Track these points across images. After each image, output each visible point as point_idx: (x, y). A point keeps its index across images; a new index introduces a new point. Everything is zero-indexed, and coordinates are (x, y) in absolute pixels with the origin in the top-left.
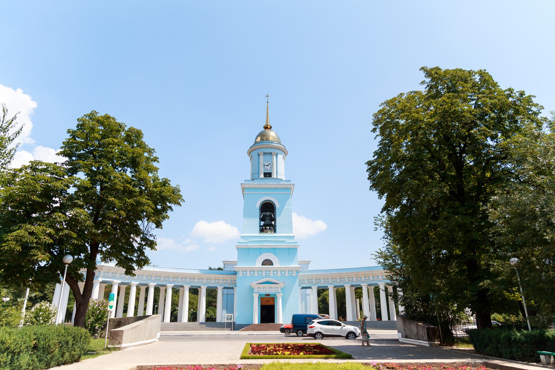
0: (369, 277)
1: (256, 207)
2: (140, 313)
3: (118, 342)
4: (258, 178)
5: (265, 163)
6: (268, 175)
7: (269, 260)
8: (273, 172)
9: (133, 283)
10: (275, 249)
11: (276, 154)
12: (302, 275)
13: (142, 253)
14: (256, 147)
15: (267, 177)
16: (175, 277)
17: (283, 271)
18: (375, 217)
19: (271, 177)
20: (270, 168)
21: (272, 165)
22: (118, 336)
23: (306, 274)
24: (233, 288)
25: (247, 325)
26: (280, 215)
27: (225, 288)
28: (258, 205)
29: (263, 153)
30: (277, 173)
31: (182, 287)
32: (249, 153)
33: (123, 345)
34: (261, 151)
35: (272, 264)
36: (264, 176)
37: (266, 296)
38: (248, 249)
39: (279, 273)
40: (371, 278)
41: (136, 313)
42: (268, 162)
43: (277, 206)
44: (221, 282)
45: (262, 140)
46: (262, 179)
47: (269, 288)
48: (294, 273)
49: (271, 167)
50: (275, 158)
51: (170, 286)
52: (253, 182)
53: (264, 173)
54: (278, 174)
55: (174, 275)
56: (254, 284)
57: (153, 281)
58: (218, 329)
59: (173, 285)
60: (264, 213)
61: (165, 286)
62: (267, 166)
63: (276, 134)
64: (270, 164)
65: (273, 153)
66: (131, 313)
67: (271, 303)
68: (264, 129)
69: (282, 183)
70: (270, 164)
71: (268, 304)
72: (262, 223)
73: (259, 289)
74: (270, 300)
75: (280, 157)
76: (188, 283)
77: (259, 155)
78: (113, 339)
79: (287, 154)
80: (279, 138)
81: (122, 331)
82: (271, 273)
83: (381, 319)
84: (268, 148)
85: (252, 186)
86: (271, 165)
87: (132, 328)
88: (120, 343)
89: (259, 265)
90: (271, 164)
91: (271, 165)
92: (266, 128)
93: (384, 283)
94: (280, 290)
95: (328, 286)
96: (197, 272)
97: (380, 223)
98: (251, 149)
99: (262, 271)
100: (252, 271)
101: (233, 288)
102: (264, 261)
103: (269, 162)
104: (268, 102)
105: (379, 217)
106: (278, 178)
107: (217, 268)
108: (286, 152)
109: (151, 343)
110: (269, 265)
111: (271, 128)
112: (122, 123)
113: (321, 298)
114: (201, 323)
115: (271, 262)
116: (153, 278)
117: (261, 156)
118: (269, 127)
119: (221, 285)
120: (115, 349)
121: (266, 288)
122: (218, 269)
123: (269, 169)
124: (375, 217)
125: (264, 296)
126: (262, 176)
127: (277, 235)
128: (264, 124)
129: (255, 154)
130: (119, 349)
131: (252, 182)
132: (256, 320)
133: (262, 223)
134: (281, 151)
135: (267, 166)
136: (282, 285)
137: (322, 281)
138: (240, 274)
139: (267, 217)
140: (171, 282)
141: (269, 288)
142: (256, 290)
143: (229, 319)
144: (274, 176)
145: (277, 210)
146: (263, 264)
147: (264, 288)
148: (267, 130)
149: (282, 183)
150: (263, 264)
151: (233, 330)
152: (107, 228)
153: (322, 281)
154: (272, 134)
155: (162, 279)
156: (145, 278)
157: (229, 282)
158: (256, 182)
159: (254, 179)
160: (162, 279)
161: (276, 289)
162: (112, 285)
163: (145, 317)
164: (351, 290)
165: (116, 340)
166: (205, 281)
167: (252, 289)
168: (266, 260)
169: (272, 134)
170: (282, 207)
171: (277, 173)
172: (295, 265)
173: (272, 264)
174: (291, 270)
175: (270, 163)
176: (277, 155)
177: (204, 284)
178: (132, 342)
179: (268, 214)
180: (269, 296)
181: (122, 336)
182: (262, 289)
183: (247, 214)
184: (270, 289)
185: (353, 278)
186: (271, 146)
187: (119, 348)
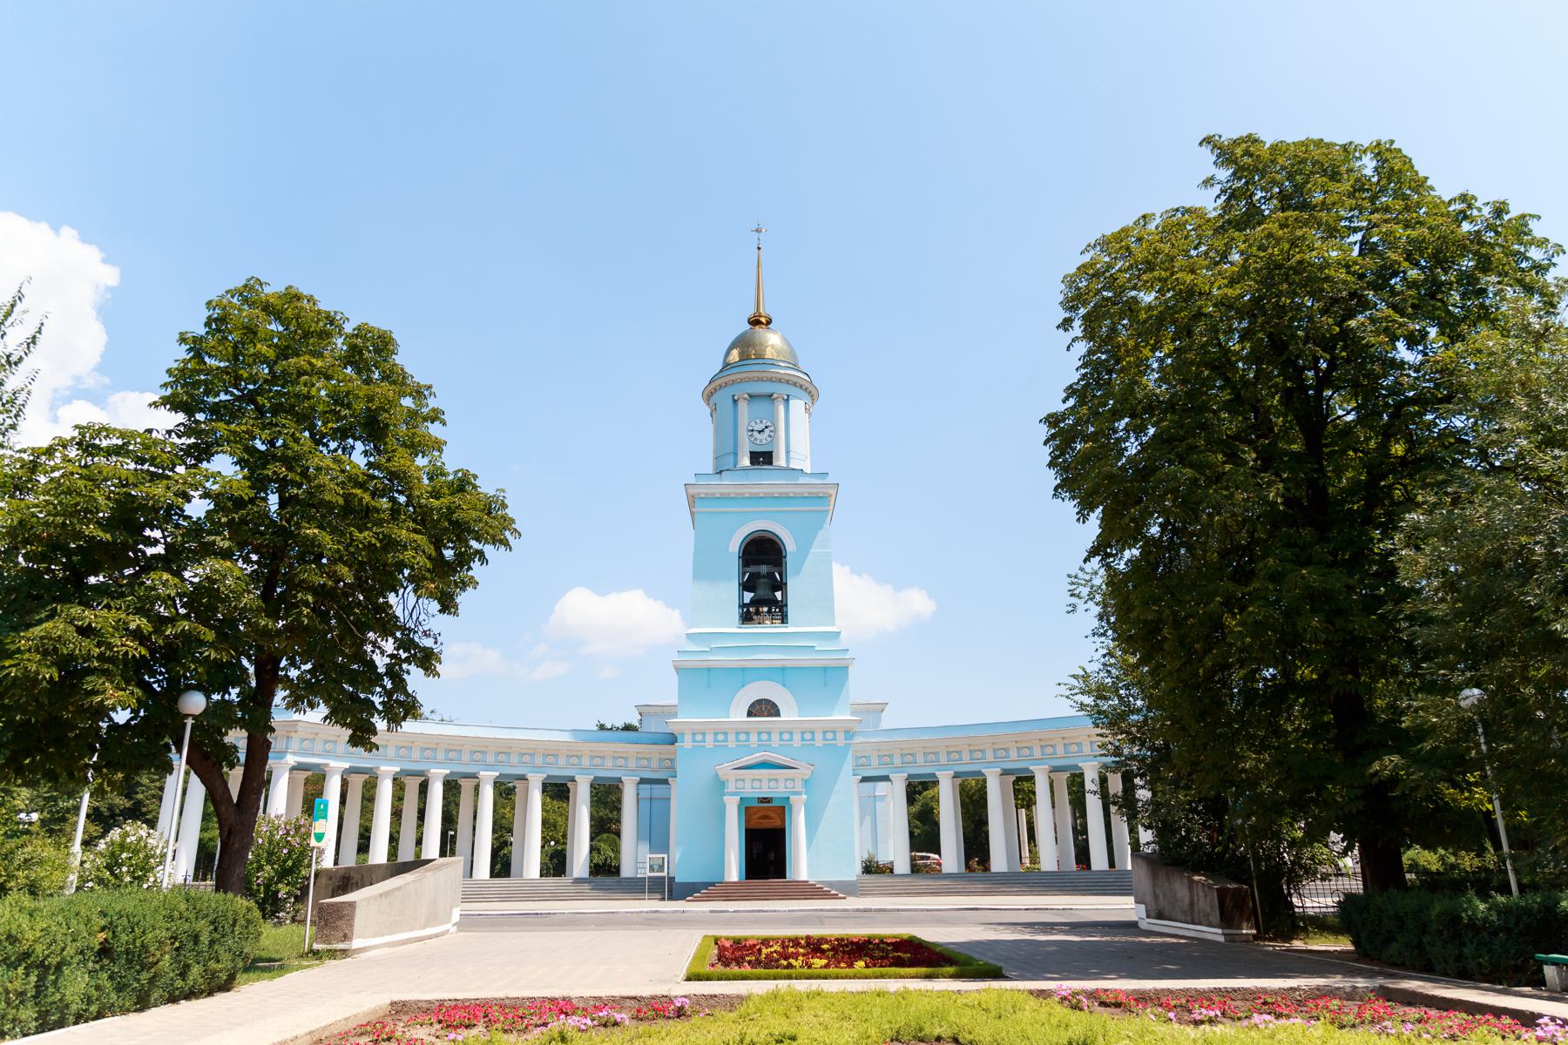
0: (1030, 748)
1: (731, 550)
2: (406, 854)
3: (341, 934)
4: (734, 468)
5: (753, 424)
6: (762, 458)
7: (768, 702)
8: (778, 452)
9: (382, 768)
10: (784, 669)
11: (786, 397)
12: (861, 743)
13: (400, 684)
14: (723, 380)
15: (759, 464)
16: (501, 750)
17: (808, 732)
18: (1069, 576)
19: (770, 463)
20: (769, 439)
21: (775, 431)
22: (340, 918)
23: (874, 740)
24: (665, 782)
25: (706, 885)
26: (798, 572)
27: (643, 781)
28: (735, 546)
29: (746, 396)
30: (788, 452)
31: (523, 778)
32: (708, 395)
33: (356, 943)
34: (742, 390)
35: (778, 714)
36: (752, 463)
37: (762, 802)
38: (709, 669)
39: (797, 737)
40: (1060, 751)
41: (393, 851)
42: (761, 422)
43: (790, 546)
44: (632, 764)
45: (744, 357)
46: (744, 469)
47: (770, 780)
48: (840, 736)
49: (770, 436)
50: (781, 408)
51: (488, 778)
52: (721, 480)
53: (751, 453)
54: (792, 455)
55: (449, 744)
56: (725, 770)
57: (440, 764)
58: (626, 896)
59: (497, 774)
60: (753, 569)
61: (474, 776)
62: (760, 432)
63: (784, 339)
64: (766, 427)
65: (775, 396)
66: (379, 853)
67: (776, 823)
68: (749, 326)
69: (802, 480)
70: (766, 427)
71: (766, 824)
72: (748, 596)
73: (740, 784)
74: (771, 814)
75: (797, 405)
76: (537, 768)
77: (735, 401)
78: (326, 925)
79: (815, 397)
80: (792, 352)
81: (352, 905)
82: (775, 737)
83: (1089, 867)
84: (750, 380)
85: (718, 491)
86: (772, 428)
87: (381, 895)
88: (346, 938)
89: (739, 715)
90: (769, 428)
91: (772, 428)
92: (755, 322)
93: (1046, 767)
94: (799, 787)
95: (937, 773)
96: (566, 737)
97: (1085, 591)
98: (713, 385)
99: (747, 733)
100: (721, 732)
101: (665, 782)
102: (753, 705)
103: (764, 421)
104: (759, 248)
105: (1081, 575)
106: (792, 466)
107: (620, 724)
108: (814, 392)
109: (436, 936)
110: (768, 716)
111: (769, 322)
112: (336, 313)
113: (916, 808)
114: (579, 881)
115: (774, 706)
116: (441, 756)
117: (743, 406)
118: (763, 320)
119: (632, 772)
120: (332, 954)
121: (760, 780)
122: (623, 729)
123: (764, 442)
124: (1069, 576)
125: (755, 804)
126: (746, 462)
127: (789, 629)
128: (750, 312)
129: (723, 397)
130: (345, 953)
131: (716, 481)
132: (734, 870)
133: (748, 596)
134: (793, 388)
135: (760, 432)
136: (804, 771)
137: (920, 759)
138: (686, 743)
139: (762, 580)
140: (490, 767)
141: (770, 780)
142: (731, 787)
143: (656, 867)
144: (780, 460)
145: (789, 560)
146: (750, 714)
147: (753, 780)
148: (757, 327)
149: (802, 480)
150: (750, 714)
151: (669, 899)
152: (301, 612)
153: (920, 759)
154: (772, 340)
155: (466, 757)
156: (416, 755)
157: (654, 765)
158: (727, 479)
159: (721, 472)
160: (466, 757)
161: (789, 784)
162: (325, 776)
163: (418, 863)
164: (1002, 784)
165: (335, 928)
166: (586, 762)
167: (720, 785)
168: (759, 702)
169: (772, 340)
170: (804, 550)
171: (788, 452)
172: (841, 715)
173: (778, 714)
174: (831, 730)
175: (769, 424)
176: (787, 401)
177: (584, 770)
178: (383, 935)
179: (764, 569)
180: (769, 802)
181: (352, 917)
182: (748, 785)
183: (703, 571)
184: (773, 784)
185: (1081, 743)
186: (769, 375)
187: (344, 951)
